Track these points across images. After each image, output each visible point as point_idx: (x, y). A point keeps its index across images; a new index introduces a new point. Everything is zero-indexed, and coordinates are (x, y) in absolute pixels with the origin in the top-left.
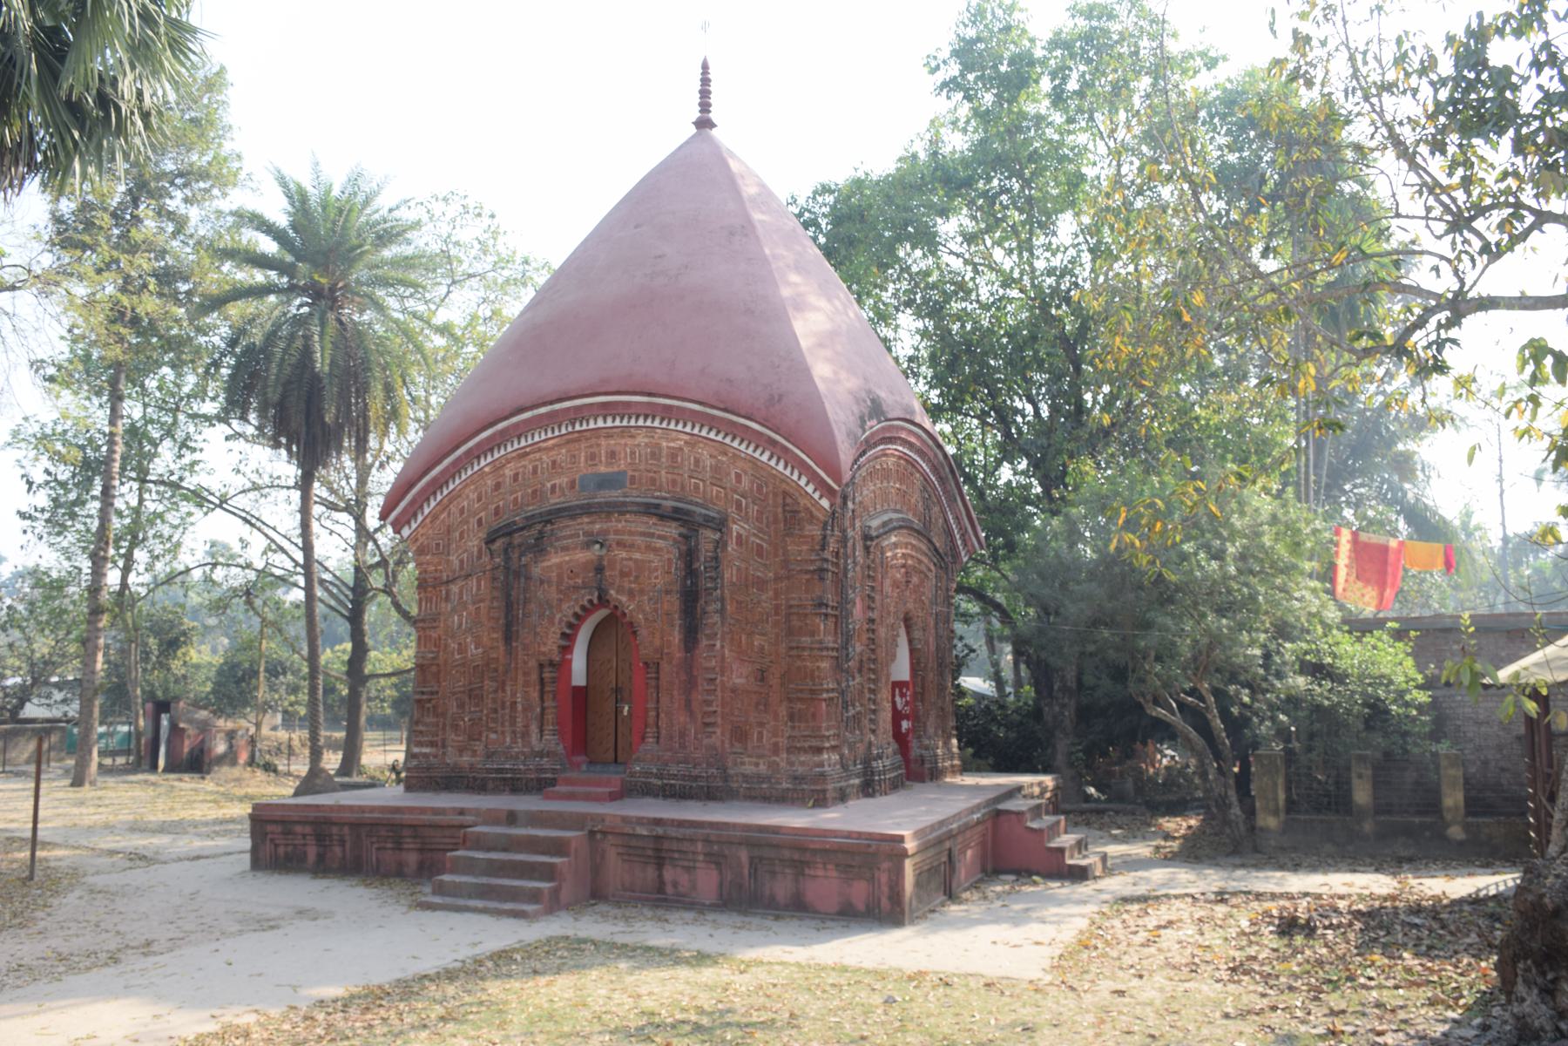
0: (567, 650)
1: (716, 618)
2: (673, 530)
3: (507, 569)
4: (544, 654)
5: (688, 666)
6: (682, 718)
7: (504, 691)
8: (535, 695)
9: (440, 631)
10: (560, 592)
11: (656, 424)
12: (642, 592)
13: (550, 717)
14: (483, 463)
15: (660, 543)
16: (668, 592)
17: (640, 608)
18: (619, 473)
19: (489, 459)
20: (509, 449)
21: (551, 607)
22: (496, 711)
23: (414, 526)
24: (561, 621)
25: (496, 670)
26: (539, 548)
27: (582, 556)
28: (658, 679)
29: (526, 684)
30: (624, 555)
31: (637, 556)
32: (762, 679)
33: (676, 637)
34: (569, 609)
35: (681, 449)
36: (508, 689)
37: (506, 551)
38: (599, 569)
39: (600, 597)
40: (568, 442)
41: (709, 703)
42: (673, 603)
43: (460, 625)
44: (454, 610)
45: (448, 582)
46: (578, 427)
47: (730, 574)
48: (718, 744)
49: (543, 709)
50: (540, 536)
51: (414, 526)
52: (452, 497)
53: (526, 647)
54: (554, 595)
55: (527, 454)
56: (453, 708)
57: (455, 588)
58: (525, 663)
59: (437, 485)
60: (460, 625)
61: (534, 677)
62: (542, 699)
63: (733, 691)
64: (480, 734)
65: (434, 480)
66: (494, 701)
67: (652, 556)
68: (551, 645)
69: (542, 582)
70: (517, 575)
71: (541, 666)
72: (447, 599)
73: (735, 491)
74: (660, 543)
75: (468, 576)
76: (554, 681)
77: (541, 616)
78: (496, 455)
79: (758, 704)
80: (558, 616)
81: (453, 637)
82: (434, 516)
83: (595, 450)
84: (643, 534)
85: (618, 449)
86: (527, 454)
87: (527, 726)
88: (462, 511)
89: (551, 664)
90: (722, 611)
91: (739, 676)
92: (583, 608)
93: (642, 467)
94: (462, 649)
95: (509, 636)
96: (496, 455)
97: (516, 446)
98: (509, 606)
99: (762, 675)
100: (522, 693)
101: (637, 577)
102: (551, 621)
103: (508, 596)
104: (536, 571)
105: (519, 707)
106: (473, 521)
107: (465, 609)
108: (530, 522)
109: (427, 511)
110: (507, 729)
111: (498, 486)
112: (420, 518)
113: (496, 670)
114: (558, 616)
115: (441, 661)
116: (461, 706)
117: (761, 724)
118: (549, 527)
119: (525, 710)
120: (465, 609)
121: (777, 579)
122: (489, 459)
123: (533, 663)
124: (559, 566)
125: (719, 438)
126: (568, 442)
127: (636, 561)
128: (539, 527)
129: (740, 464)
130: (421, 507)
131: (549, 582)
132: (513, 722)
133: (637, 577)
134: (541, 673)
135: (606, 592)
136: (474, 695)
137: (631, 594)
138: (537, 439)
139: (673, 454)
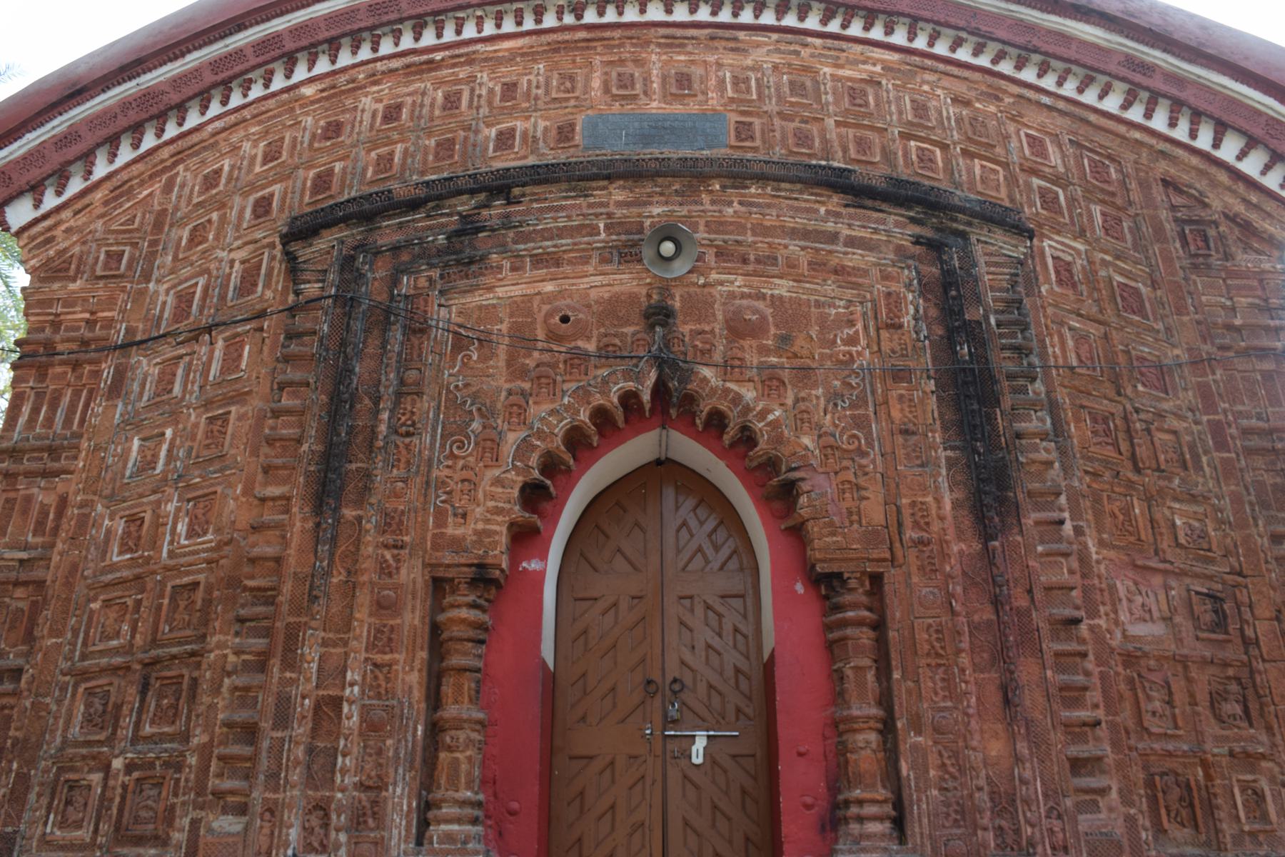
0: (526, 538)
1: (1045, 451)
2: (895, 228)
3: (346, 302)
4: (457, 545)
5: (989, 577)
6: (990, 746)
7: (291, 661)
8: (411, 679)
9: (71, 486)
10: (517, 371)
11: (812, 23)
12: (804, 374)
13: (463, 755)
14: (301, 73)
15: (856, 258)
16: (899, 375)
17: (802, 418)
18: (703, 115)
19: (323, 66)
20: (386, 47)
21: (487, 414)
22: (250, 732)
23: (50, 201)
24: (524, 448)
25: (267, 596)
26: (463, 256)
27: (600, 283)
28: (879, 626)
29: (383, 639)
30: (739, 283)
31: (783, 288)
32: (1220, 623)
33: (944, 498)
34: (552, 416)
35: (873, 82)
36: (311, 653)
37: (347, 263)
38: (659, 315)
39: (660, 390)
40: (556, 48)
41: (1072, 696)
42: (924, 401)
43: (148, 463)
44: (132, 423)
45: (126, 346)
46: (590, 17)
47: (1061, 348)
48: (1119, 830)
49: (435, 729)
50: (469, 227)
51: (50, 201)
52: (184, 149)
53: (390, 522)
54: (497, 380)
55: (432, 65)
56: (70, 720)
57: (146, 366)
58: (386, 570)
59: (156, 109)
60: (148, 463)
61: (413, 618)
62: (434, 699)
63: (1130, 659)
64: (169, 817)
65: (148, 96)
66: (244, 695)
67: (830, 288)
68: (486, 515)
69: (460, 343)
70: (384, 317)
71: (439, 585)
72: (117, 388)
73: (1034, 172)
74: (856, 258)
75: (196, 334)
76: (481, 635)
77: (455, 433)
78: (345, 59)
79: (1215, 700)
80: (512, 438)
81: (112, 499)
82: (120, 187)
83: (629, 68)
84: (805, 234)
85: (697, 71)
86: (432, 65)
87: (374, 787)
88: (211, 180)
89: (483, 578)
90: (1058, 430)
91: (1141, 616)
92: (601, 416)
93: (771, 106)
94: (138, 534)
95: (330, 485)
96: (345, 59)
97: (407, 42)
98: (340, 401)
99: (1218, 612)
100: (364, 665)
101: (785, 339)
102: (490, 447)
103: (342, 374)
104: (445, 314)
105: (352, 717)
106: (242, 207)
107: (174, 417)
108: (432, 197)
109: (101, 169)
110: (295, 794)
111: (334, 129)
112: (75, 186)
113: (267, 596)
114: (512, 438)
115: (52, 574)
116: (105, 717)
117: (1249, 760)
118: (497, 209)
119: (371, 727)
120: (174, 417)
121: (1197, 363)
122: (323, 66)
123: (412, 574)
124: (521, 307)
125: (984, 61)
126: (556, 48)
127: (776, 301)
128: (464, 205)
129: (1035, 118)
130: (88, 158)
131: (485, 342)
132: (321, 766)
133: (785, 339)
134: (438, 606)
135: (686, 375)
136: (163, 677)
137: (771, 382)
138: (470, 32)
139: (855, 93)
